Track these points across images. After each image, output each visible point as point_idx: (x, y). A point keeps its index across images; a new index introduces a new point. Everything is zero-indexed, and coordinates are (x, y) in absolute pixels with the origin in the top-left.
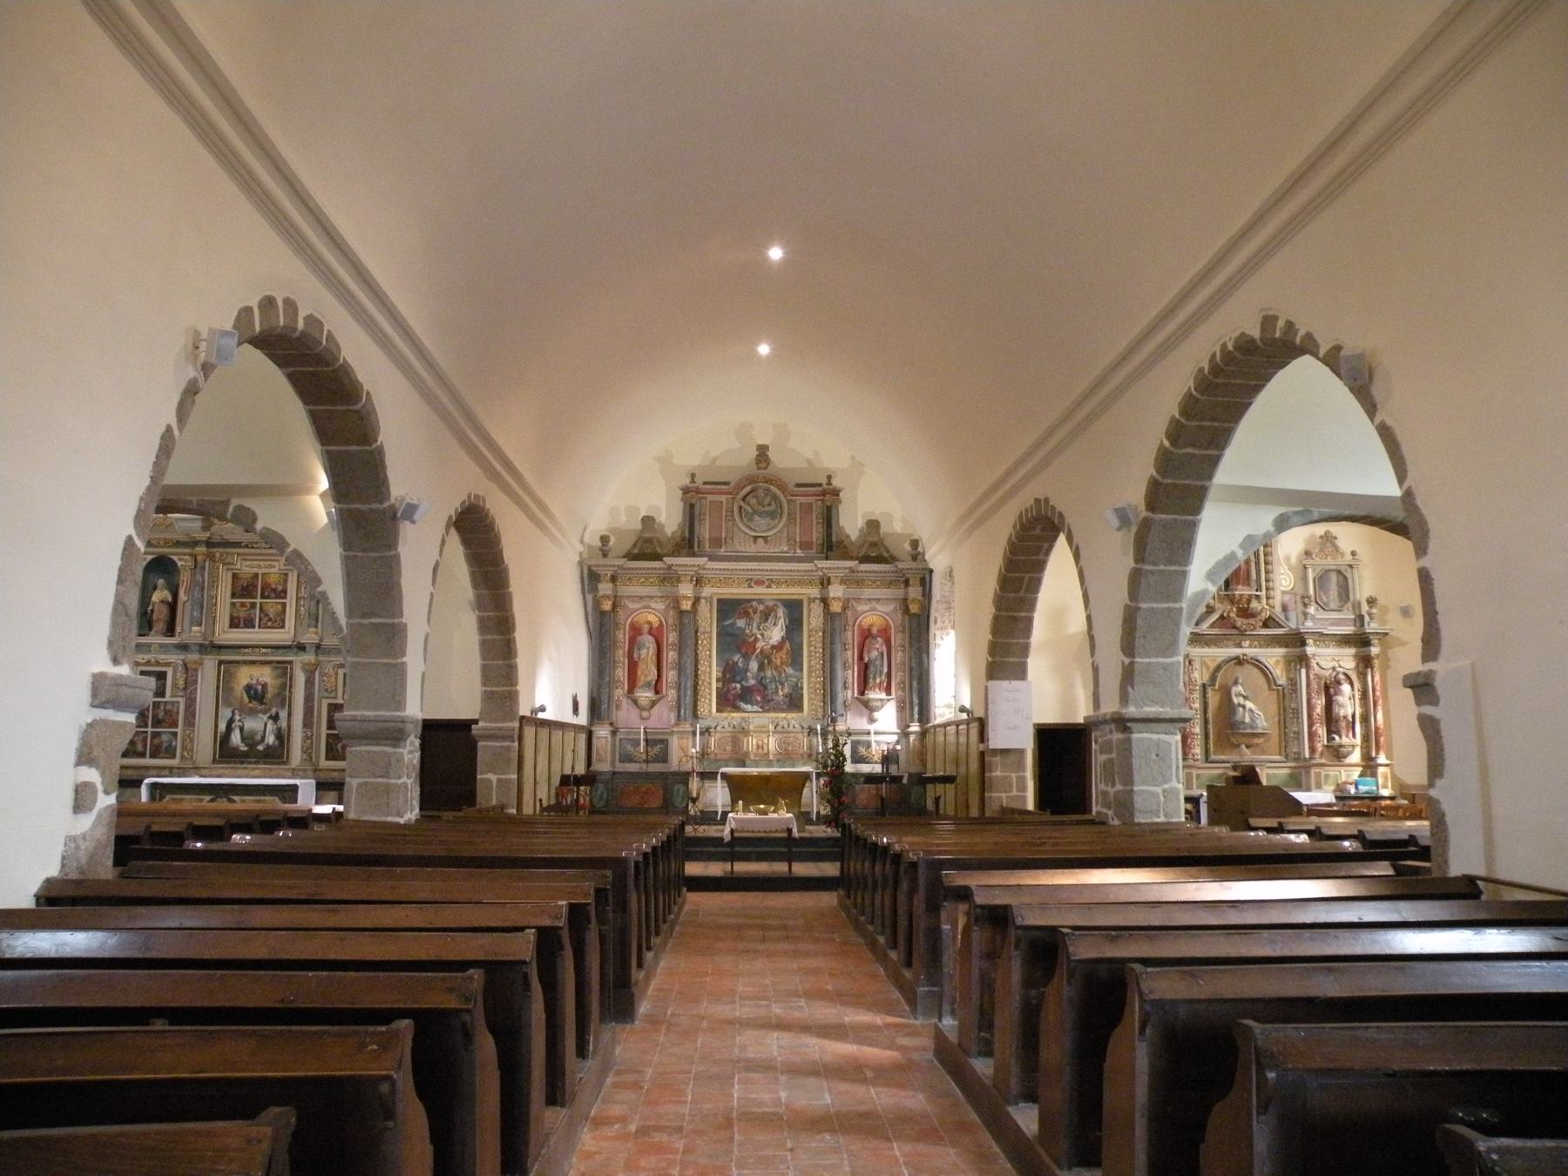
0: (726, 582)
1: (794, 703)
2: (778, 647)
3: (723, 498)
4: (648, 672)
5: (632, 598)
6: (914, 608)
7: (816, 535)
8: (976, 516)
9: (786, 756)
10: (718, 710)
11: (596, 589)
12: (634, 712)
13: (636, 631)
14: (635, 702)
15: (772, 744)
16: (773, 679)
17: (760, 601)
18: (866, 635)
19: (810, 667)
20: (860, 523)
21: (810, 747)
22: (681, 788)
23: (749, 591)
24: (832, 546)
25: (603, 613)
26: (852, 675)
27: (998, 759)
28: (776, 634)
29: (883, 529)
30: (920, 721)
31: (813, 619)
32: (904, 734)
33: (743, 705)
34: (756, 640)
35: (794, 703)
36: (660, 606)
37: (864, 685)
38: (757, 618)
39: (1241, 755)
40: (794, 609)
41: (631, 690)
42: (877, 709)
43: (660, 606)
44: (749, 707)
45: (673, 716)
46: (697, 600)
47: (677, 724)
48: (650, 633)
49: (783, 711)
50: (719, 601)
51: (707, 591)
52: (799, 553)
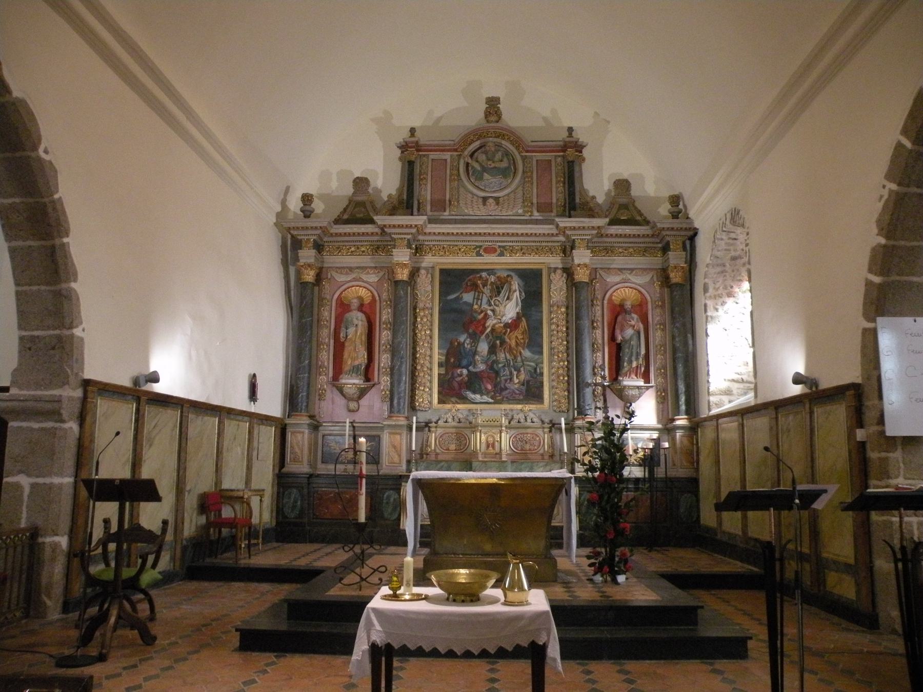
0: (446, 250)
1: (532, 392)
2: (513, 325)
3: (447, 156)
4: (356, 355)
5: (340, 269)
6: (676, 277)
7: (557, 194)
8: (793, 101)
9: (521, 457)
10: (441, 401)
11: (296, 259)
12: (340, 401)
13: (343, 307)
14: (341, 390)
15: (505, 441)
16: (507, 364)
17: (491, 272)
18: (618, 311)
19: (551, 349)
20: (607, 185)
21: (552, 445)
22: (393, 495)
24: (575, 204)
25: (303, 285)
26: (603, 357)
27: (897, 455)
28: (510, 310)
29: (635, 192)
30: (687, 412)
31: (555, 291)
32: (667, 428)
33: (471, 395)
34: (486, 317)
35: (532, 392)
36: (373, 278)
37: (617, 370)
40: (532, 281)
41: (336, 377)
42: (636, 398)
43: (373, 278)
44: (478, 397)
45: (386, 407)
46: (414, 273)
47: (390, 417)
48: (361, 308)
49: (519, 402)
50: (442, 271)
51: (429, 260)
52: (537, 215)
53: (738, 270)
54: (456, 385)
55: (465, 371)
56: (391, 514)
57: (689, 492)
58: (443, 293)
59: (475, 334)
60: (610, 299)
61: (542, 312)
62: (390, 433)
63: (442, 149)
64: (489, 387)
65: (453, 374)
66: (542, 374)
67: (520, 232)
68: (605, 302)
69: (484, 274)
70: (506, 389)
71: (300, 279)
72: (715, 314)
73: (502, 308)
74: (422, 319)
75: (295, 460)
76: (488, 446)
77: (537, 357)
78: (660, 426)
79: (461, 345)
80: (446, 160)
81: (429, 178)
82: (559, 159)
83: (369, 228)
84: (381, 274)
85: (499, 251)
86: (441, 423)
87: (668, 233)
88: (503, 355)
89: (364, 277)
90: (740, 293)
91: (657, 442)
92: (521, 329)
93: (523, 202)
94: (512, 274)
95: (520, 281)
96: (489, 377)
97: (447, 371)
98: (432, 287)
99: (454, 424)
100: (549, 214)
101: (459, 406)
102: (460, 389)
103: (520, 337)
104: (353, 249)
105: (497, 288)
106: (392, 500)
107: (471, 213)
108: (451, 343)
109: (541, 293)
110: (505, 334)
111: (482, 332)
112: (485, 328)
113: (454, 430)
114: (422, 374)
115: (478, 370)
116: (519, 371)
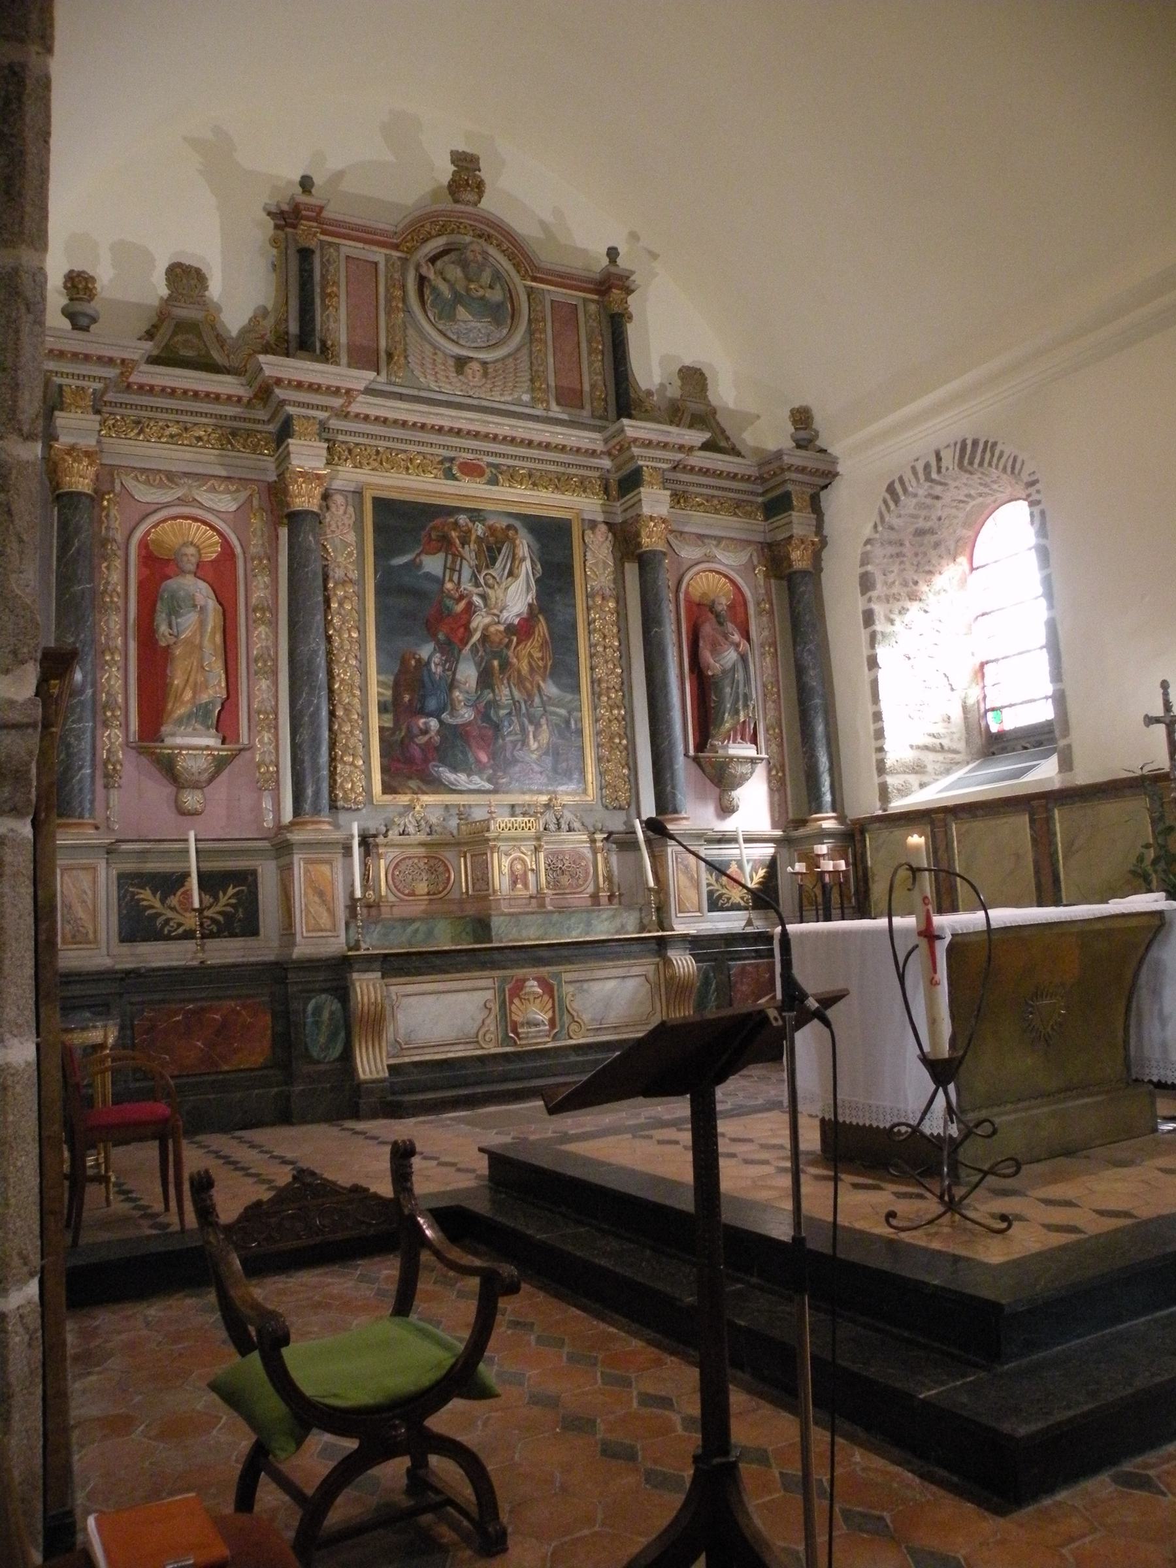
0: (381, 459)
2: (522, 630)
3: (378, 255)
4: (197, 679)
5: (149, 475)
7: (592, 375)
10: (387, 789)
12: (157, 791)
13: (157, 566)
14: (168, 768)
17: (476, 515)
18: (700, 613)
23: (448, 487)
24: (624, 400)
28: (516, 598)
31: (595, 560)
33: (448, 775)
34: (470, 609)
36: (225, 502)
43: (225, 502)
50: (378, 502)
52: (556, 411)
53: (925, 554)
54: (417, 752)
55: (434, 723)
56: (325, 1048)
57: (324, 991)
59: (449, 642)
60: (687, 593)
61: (574, 606)
62: (308, 862)
63: (367, 235)
64: (484, 757)
65: (409, 730)
67: (537, 438)
68: (682, 596)
71: (58, 486)
72: (889, 629)
73: (500, 593)
74: (341, 604)
75: (79, 938)
76: (515, 883)
77: (569, 697)
78: (778, 833)
79: (423, 665)
80: (376, 264)
81: (343, 296)
82: (593, 308)
83: (226, 385)
84: (243, 495)
86: (393, 835)
87: (794, 476)
88: (506, 691)
89: (204, 497)
90: (930, 595)
91: (772, 866)
93: (532, 381)
94: (518, 524)
95: (529, 536)
97: (396, 721)
99: (422, 837)
100: (577, 411)
101: (427, 799)
102: (426, 761)
103: (537, 655)
104: (174, 430)
105: (490, 549)
106: (326, 1015)
107: (433, 386)
108: (404, 662)
110: (508, 646)
111: (464, 641)
112: (469, 633)
113: (421, 851)
114: (347, 728)
115: (459, 721)
116: (538, 726)
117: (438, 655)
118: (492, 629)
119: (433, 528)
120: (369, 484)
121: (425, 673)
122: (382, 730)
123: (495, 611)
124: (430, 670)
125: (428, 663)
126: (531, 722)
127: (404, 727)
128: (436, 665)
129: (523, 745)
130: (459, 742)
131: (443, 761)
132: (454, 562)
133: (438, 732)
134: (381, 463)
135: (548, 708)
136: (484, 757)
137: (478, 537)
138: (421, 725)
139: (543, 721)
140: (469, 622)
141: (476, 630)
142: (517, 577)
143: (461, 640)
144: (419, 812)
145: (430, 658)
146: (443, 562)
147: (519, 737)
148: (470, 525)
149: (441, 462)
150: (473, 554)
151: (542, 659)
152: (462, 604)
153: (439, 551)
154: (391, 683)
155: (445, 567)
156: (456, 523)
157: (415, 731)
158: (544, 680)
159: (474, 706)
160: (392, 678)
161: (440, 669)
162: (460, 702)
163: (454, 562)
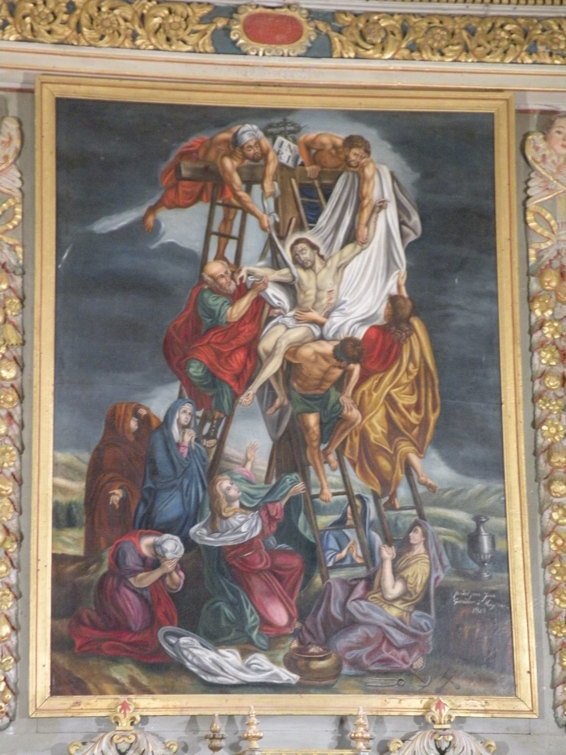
2: (375, 350)
10: (63, 683)
16: (353, 513)
17: (278, 121)
28: (361, 285)
33: (197, 653)
38: (261, 201)
39: (311, 301)
44: (228, 661)
49: (401, 679)
50: (67, 109)
54: (132, 607)
55: (172, 546)
58: (72, 211)
59: (212, 378)
61: (494, 296)
64: (279, 614)
66: (502, 561)
69: (249, 132)
70: (351, 623)
73: (326, 276)
77: (478, 485)
85: (309, 32)
88: (335, 477)
92: (405, 370)
94: (370, 134)
96: (276, 572)
97: (91, 544)
98: (27, 172)
102: (153, 623)
103: (405, 400)
105: (306, 190)
108: (113, 423)
109: (488, 218)
110: (340, 384)
111: (245, 378)
112: (255, 360)
116: (403, 546)
117: (188, 407)
118: (307, 351)
119: (184, 155)
120: (47, 72)
121: (159, 444)
122: (58, 560)
123: (315, 315)
124: (168, 440)
125: (166, 423)
126: (388, 541)
127: (107, 555)
128: (183, 428)
129: (369, 587)
130: (224, 582)
131: (191, 624)
132: (227, 221)
133: (182, 564)
134: (78, 28)
135: (429, 511)
136: (279, 614)
137: (281, 166)
138: (145, 551)
139: (416, 537)
140: (256, 339)
141: (270, 355)
142: (365, 243)
143: (238, 377)
144: (124, 734)
145: (171, 412)
146: (204, 223)
147: (361, 571)
148: (266, 142)
149: (206, 19)
150: (270, 203)
151: (417, 408)
152: (244, 304)
153: (198, 199)
154: (84, 467)
155: (208, 233)
156: (235, 142)
157: (131, 561)
158: (420, 452)
159: (261, 507)
160: (87, 457)
161: (189, 437)
162: (230, 500)
163: (227, 221)
